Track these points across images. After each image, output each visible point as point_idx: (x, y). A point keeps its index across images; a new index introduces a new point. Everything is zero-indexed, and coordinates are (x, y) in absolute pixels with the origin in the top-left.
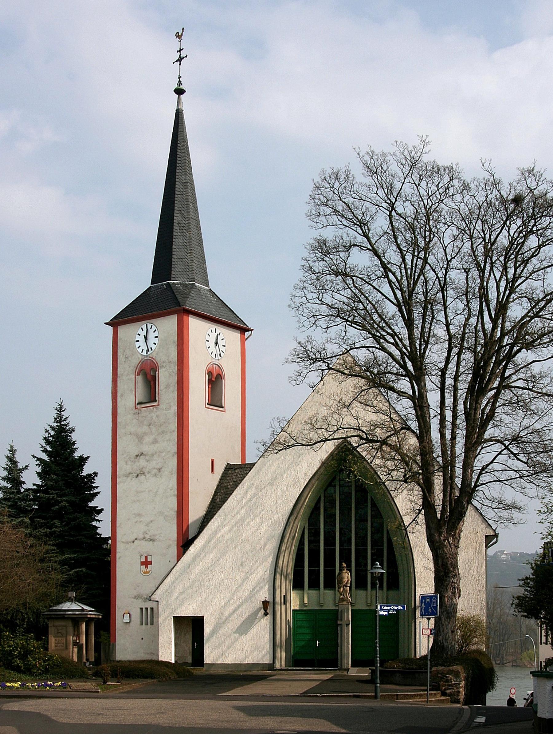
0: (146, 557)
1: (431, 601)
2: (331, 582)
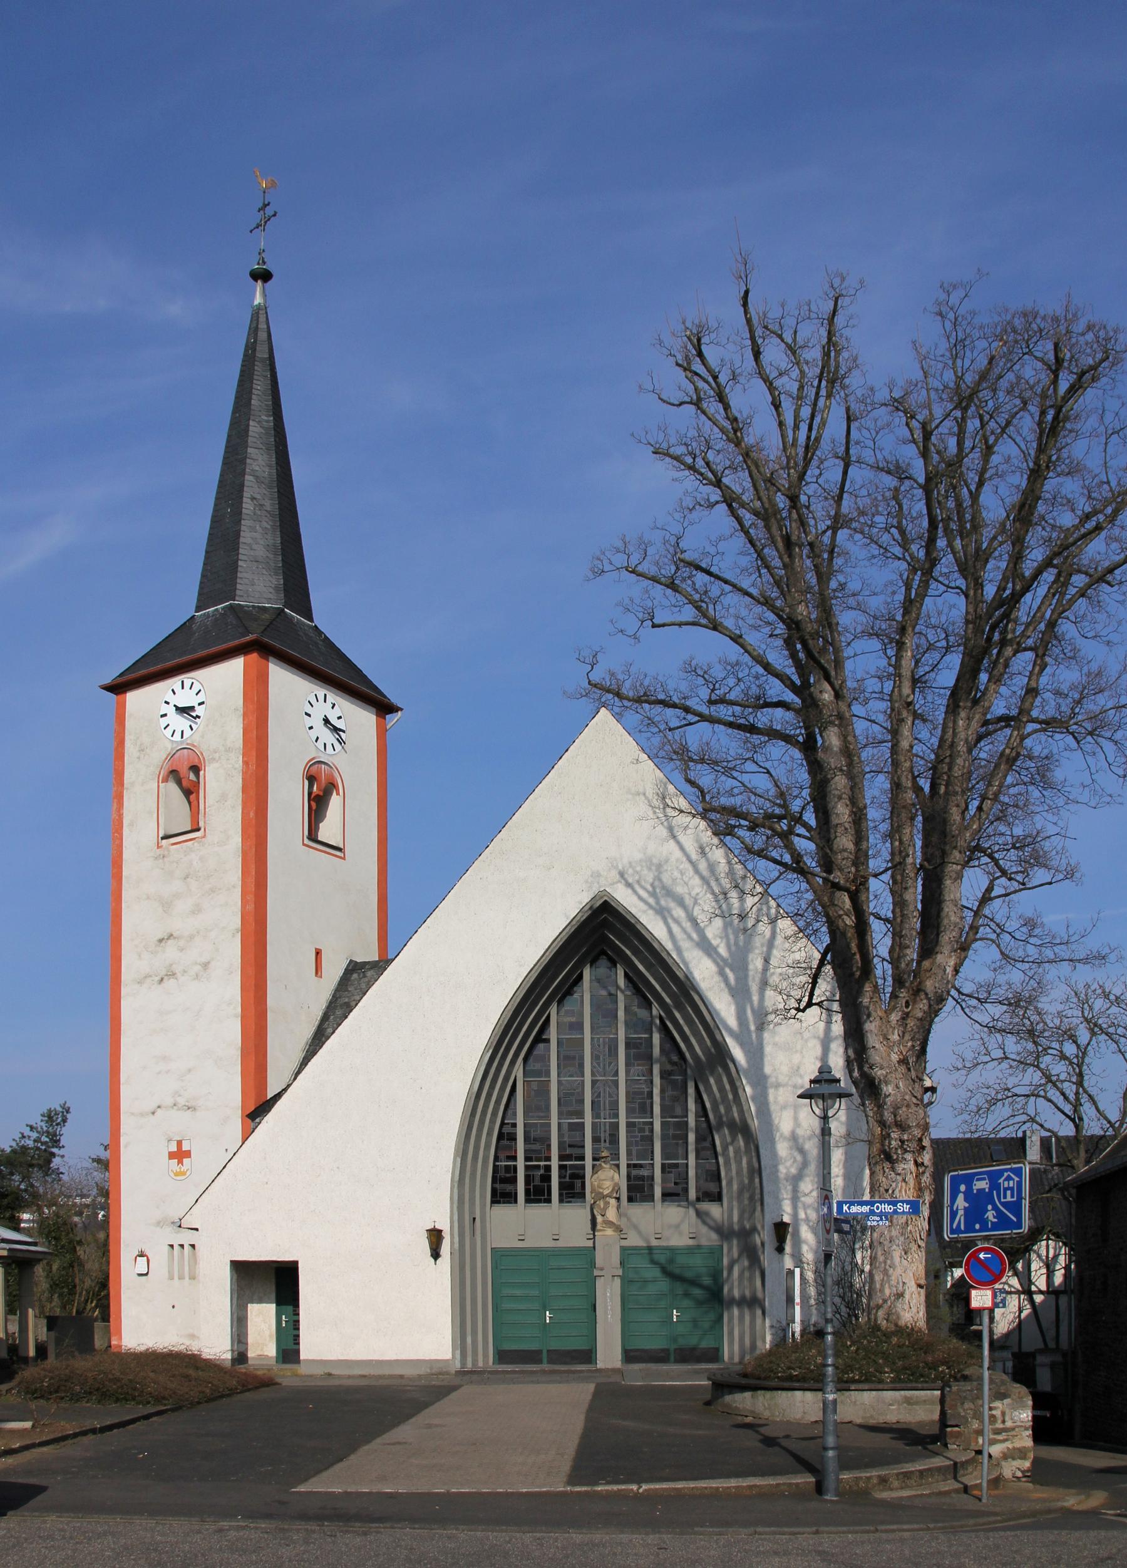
0: (179, 1143)
2: (573, 1189)
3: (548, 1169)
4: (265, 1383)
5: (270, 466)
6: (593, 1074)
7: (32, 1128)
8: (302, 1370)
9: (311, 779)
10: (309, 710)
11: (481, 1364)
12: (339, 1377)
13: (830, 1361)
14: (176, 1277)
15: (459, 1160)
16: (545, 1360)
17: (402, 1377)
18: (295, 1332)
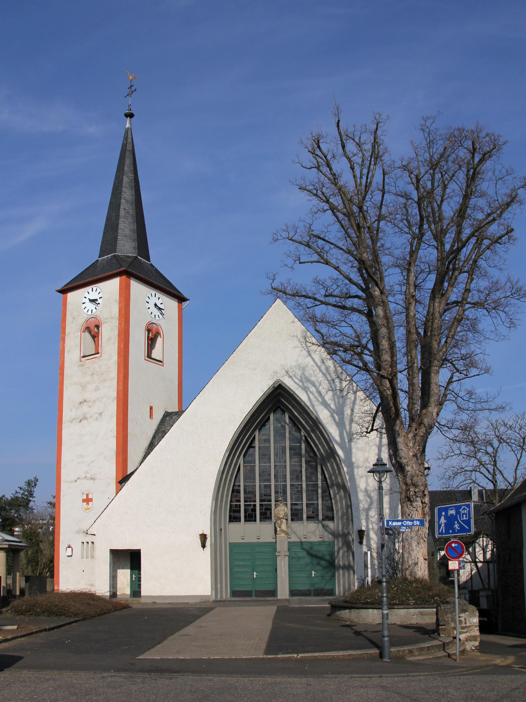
0: (87, 495)
2: (266, 515)
3: (255, 506)
5: (132, 195)
6: (275, 462)
7: (21, 488)
8: (142, 600)
9: (149, 330)
10: (148, 300)
11: (224, 597)
12: (159, 604)
14: (85, 557)
15: (214, 502)
17: (188, 603)
18: (139, 583)
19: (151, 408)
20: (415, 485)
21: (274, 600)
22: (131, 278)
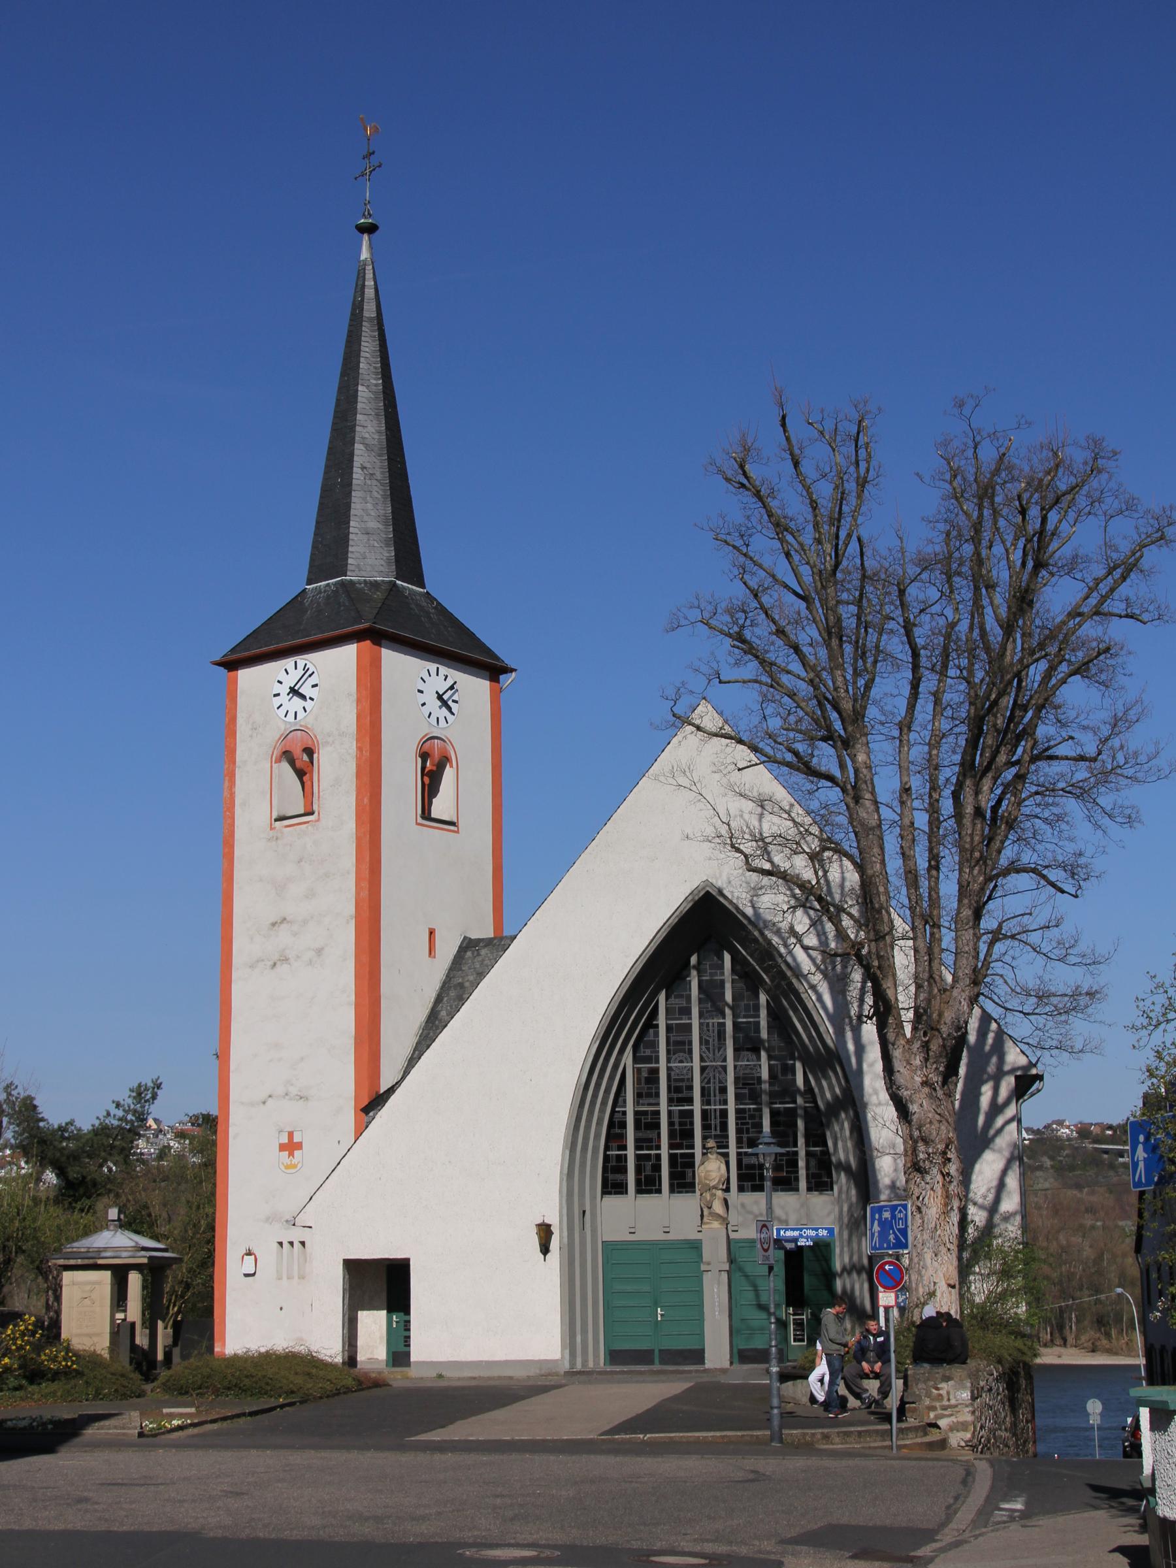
0: (291, 1135)
1: (893, 1216)
2: (683, 1181)
3: (658, 1157)
4: (376, 1383)
5: (379, 432)
6: (702, 1059)
7: (118, 1105)
8: (413, 1372)
9: (424, 756)
10: (421, 686)
11: (591, 1364)
12: (450, 1379)
13: (773, 1343)
14: (285, 1277)
15: (568, 1152)
16: (657, 1360)
17: (511, 1378)
18: (406, 1334)
19: (432, 933)
20: (926, 1141)
21: (697, 1371)
22: (383, 642)
